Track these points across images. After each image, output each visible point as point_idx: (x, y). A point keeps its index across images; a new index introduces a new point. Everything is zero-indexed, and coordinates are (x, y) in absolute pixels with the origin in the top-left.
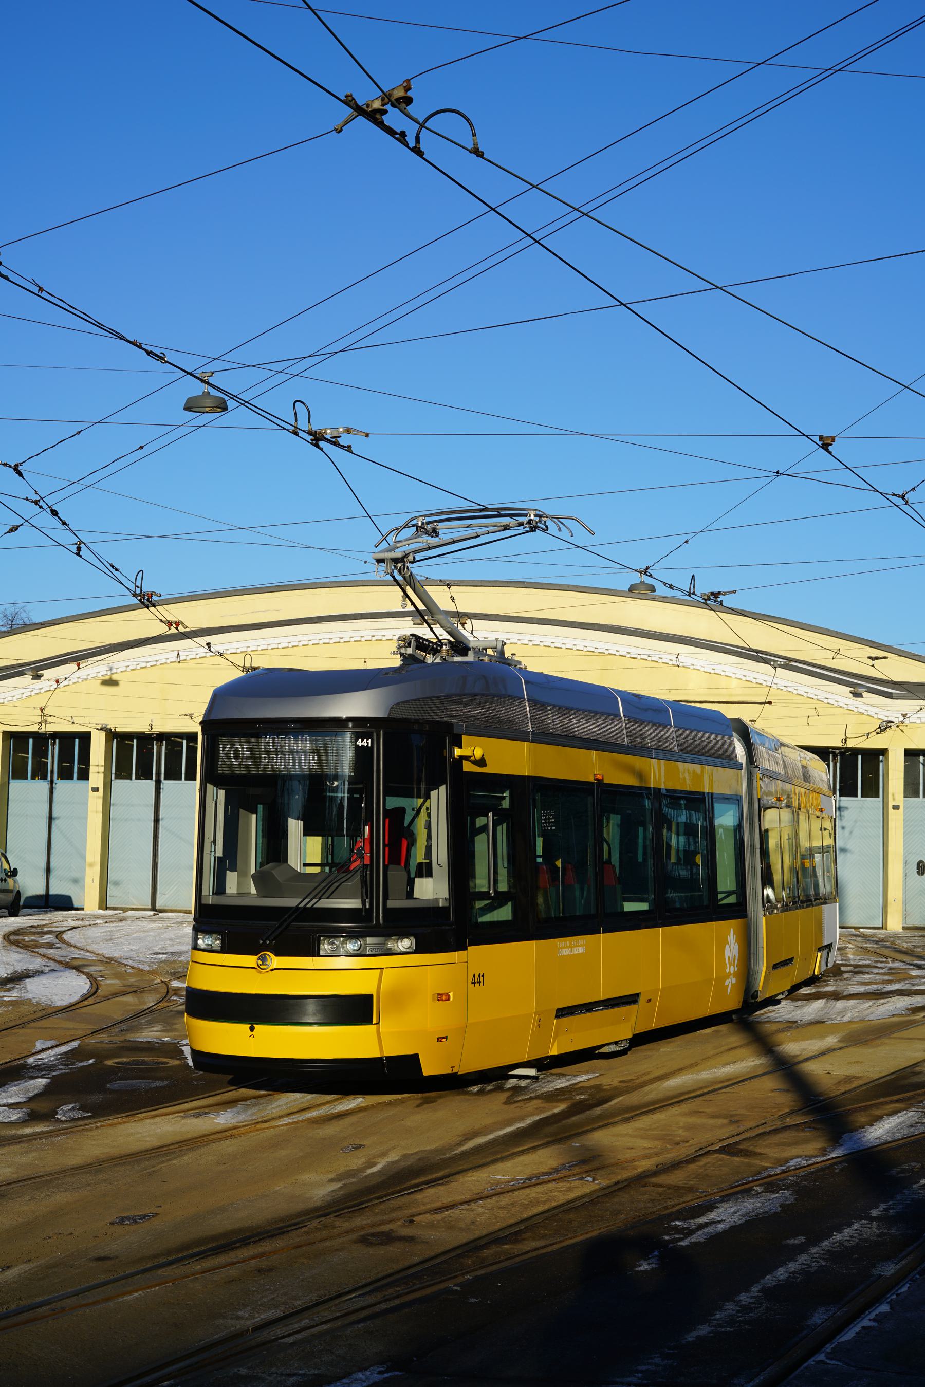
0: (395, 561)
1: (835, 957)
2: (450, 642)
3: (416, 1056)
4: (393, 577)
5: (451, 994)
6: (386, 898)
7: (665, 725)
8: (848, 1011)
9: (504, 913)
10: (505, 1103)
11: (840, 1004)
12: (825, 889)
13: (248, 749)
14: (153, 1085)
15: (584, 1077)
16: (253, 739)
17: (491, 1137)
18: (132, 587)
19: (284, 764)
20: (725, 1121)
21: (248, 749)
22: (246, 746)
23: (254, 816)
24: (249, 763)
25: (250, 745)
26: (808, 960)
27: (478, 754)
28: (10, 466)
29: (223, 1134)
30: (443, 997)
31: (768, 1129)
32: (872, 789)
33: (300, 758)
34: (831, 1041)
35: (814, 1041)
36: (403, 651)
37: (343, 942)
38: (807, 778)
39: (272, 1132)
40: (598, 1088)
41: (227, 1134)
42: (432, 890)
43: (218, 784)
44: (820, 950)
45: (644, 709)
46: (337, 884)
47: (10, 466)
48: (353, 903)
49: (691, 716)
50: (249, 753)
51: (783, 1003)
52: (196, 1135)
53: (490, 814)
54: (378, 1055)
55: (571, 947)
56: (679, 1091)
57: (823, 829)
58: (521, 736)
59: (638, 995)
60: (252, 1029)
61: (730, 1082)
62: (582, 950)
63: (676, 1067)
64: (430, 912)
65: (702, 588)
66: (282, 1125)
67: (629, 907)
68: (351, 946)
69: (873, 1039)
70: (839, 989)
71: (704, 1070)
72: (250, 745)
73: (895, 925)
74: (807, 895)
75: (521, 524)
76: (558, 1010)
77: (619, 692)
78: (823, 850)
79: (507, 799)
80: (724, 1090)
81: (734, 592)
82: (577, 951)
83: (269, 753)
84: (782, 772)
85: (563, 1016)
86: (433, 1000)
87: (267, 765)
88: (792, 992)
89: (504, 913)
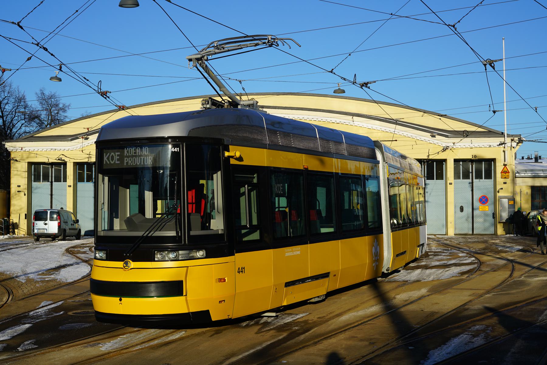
0: (198, 59)
1: (426, 248)
2: (229, 101)
3: (208, 311)
4: (197, 68)
5: (226, 279)
6: (190, 229)
7: (341, 142)
8: (432, 275)
9: (256, 236)
10: (256, 333)
11: (428, 271)
12: (420, 219)
13: (118, 155)
14: (83, 326)
15: (301, 315)
16: (120, 150)
17: (240, 357)
18: (97, 89)
19: (138, 162)
20: (367, 343)
21: (118, 155)
22: (117, 153)
23: (128, 190)
24: (119, 162)
25: (119, 153)
26: (413, 251)
27: (238, 155)
28: (15, 24)
29: (99, 358)
30: (222, 280)
31: (389, 348)
32: (440, 176)
33: (144, 159)
34: (424, 291)
35: (415, 292)
36: (205, 106)
37: (168, 254)
38: (411, 169)
39: (126, 356)
40: (306, 322)
41: (102, 357)
42: (217, 224)
43: (104, 174)
44: (418, 246)
45: (331, 136)
46: (164, 224)
47: (15, 24)
48: (173, 233)
49: (354, 140)
50: (118, 157)
51: (402, 271)
52: (84, 359)
53: (246, 186)
54: (187, 312)
55: (292, 251)
56: (346, 324)
57: (419, 194)
58: (263, 146)
59: (329, 273)
60: (121, 300)
61: (373, 317)
62: (298, 253)
63: (347, 309)
64: (216, 236)
65: (360, 80)
66: (135, 351)
67: (323, 230)
68: (172, 256)
69: (444, 290)
70: (427, 263)
71: (361, 310)
72: (119, 153)
73: (451, 233)
74: (408, 223)
75: (264, 43)
76: (286, 283)
77: (319, 128)
78: (419, 202)
79: (256, 178)
80: (369, 322)
81: (375, 82)
82: (295, 253)
83: (128, 157)
84: (399, 166)
85: (289, 286)
86: (216, 282)
87: (127, 163)
88: (406, 266)
89: (256, 236)
